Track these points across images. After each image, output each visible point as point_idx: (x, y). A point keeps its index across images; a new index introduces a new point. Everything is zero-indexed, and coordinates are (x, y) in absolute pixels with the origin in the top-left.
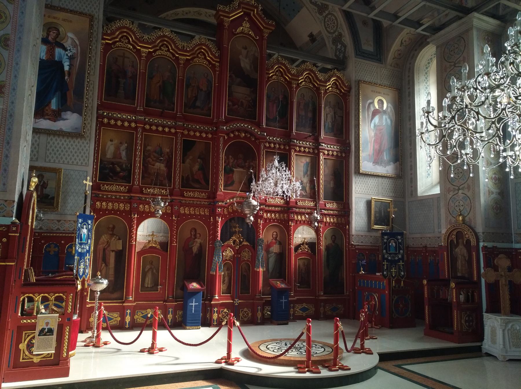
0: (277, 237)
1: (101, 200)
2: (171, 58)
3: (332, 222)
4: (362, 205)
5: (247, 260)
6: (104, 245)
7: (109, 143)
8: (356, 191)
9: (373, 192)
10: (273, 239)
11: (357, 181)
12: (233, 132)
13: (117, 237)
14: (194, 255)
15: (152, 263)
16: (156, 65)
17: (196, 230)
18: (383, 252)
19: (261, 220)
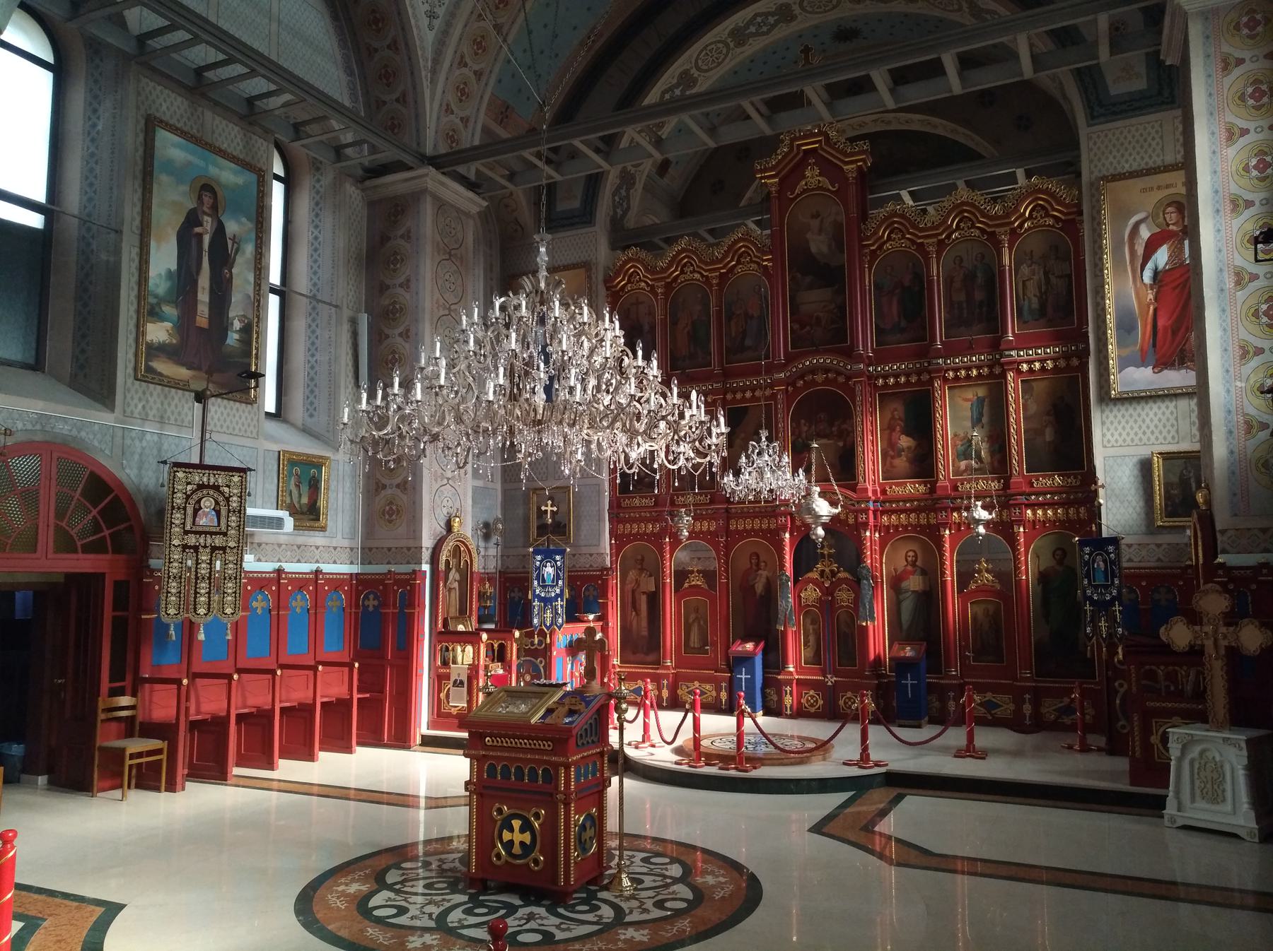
0: (916, 561)
4: (1127, 472)
11: (1107, 417)
12: (802, 377)
15: (697, 611)
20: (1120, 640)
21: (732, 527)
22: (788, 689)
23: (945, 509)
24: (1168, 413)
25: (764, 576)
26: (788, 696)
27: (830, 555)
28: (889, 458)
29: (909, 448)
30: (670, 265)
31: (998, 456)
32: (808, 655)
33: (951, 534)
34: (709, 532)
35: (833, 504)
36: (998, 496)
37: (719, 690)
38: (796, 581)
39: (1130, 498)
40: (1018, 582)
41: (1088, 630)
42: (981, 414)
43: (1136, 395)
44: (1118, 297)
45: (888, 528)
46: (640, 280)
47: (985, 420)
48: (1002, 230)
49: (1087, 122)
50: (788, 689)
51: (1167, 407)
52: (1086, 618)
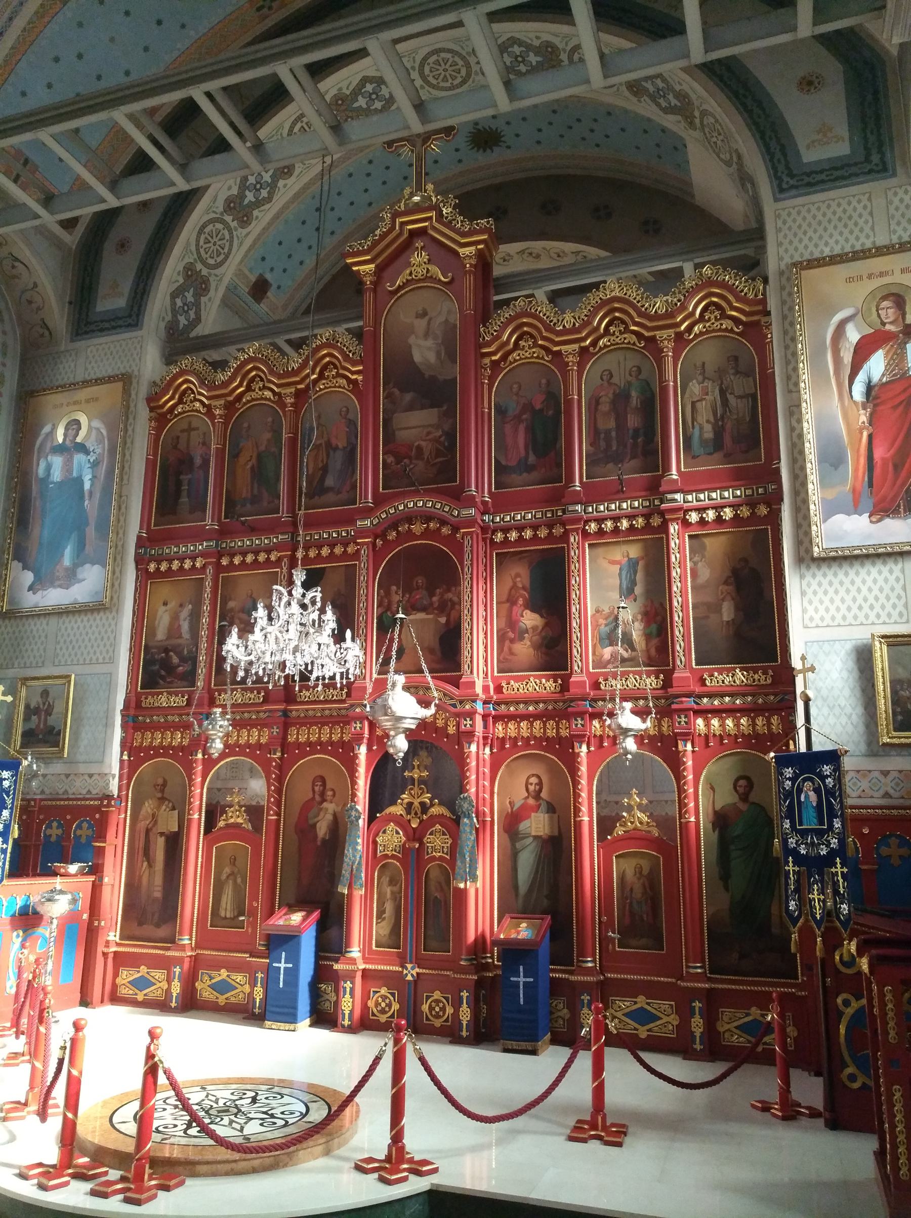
0: (540, 790)
2: (732, 331)
4: (839, 665)
7: (162, 609)
8: (807, 622)
10: (527, 798)
11: (809, 585)
13: (171, 805)
14: (319, 843)
15: (233, 861)
16: (246, 425)
17: (323, 780)
18: (782, 826)
20: (844, 925)
21: (291, 739)
22: (348, 985)
23: (581, 714)
24: (892, 578)
25: (331, 811)
26: (348, 996)
27: (422, 781)
28: (507, 643)
29: (534, 628)
30: (232, 379)
31: (655, 642)
32: (382, 932)
33: (589, 751)
34: (259, 746)
35: (424, 703)
36: (657, 698)
37: (253, 984)
38: (371, 818)
39: (843, 702)
40: (684, 826)
41: (792, 905)
42: (633, 583)
43: (847, 553)
44: (820, 420)
45: (503, 741)
46: (196, 400)
47: (638, 590)
48: (664, 334)
49: (774, 195)
50: (348, 985)
51: (891, 572)
52: (787, 884)
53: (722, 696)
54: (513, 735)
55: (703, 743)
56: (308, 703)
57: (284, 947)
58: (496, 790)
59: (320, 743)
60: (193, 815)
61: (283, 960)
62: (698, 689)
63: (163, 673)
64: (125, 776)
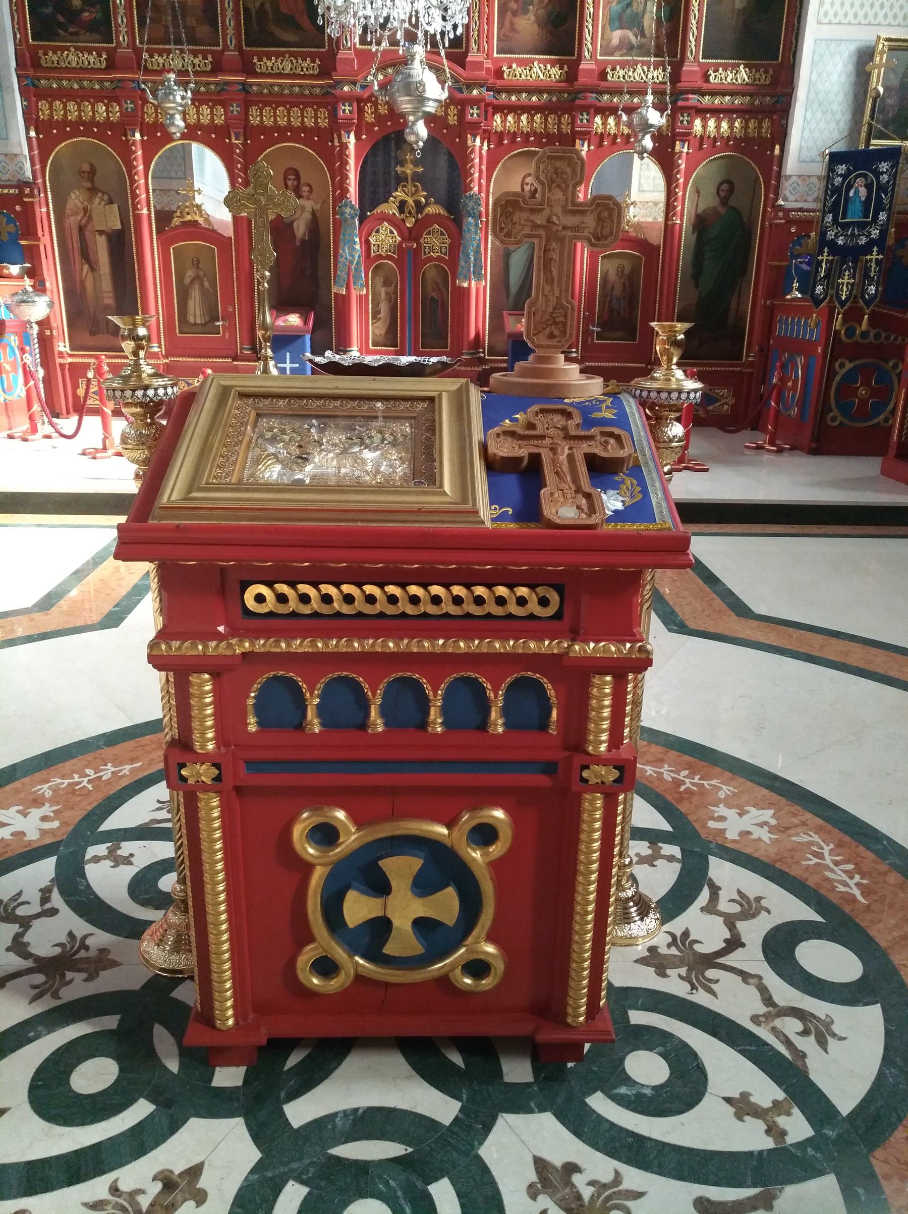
1: (50, 95)
3: (726, 135)
4: (840, 67)
5: (439, 259)
6: (79, 218)
9: (890, 15)
13: (106, 197)
14: (298, 243)
15: (197, 264)
19: (475, 136)
23: (586, 109)
27: (416, 177)
28: (509, 14)
32: (378, 332)
33: (589, 150)
38: (362, 219)
45: (501, 135)
53: (724, 94)
54: (525, 130)
55: (697, 144)
56: (270, 75)
57: (289, 347)
58: (491, 190)
59: (289, 127)
60: (141, 209)
61: (288, 361)
62: (700, 83)
63: (61, 18)
64: (37, 160)
